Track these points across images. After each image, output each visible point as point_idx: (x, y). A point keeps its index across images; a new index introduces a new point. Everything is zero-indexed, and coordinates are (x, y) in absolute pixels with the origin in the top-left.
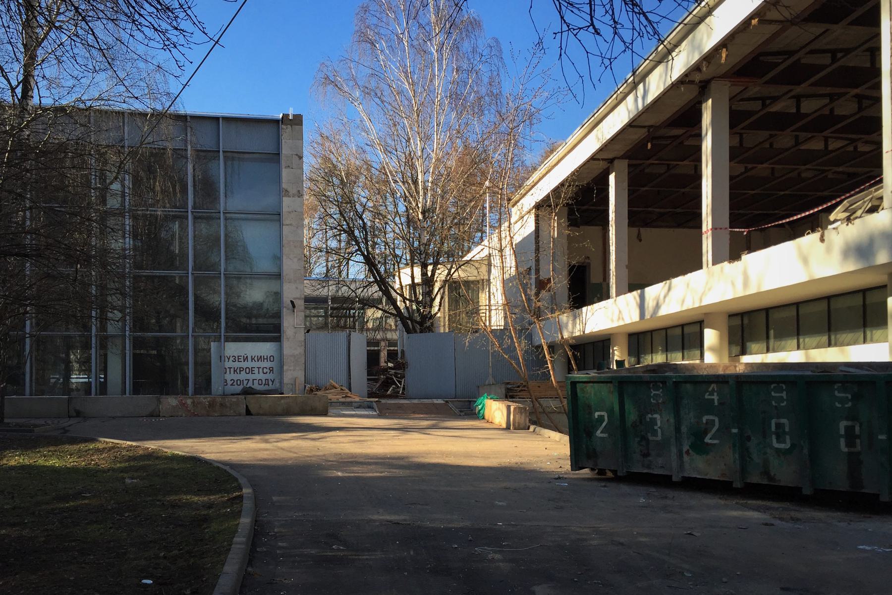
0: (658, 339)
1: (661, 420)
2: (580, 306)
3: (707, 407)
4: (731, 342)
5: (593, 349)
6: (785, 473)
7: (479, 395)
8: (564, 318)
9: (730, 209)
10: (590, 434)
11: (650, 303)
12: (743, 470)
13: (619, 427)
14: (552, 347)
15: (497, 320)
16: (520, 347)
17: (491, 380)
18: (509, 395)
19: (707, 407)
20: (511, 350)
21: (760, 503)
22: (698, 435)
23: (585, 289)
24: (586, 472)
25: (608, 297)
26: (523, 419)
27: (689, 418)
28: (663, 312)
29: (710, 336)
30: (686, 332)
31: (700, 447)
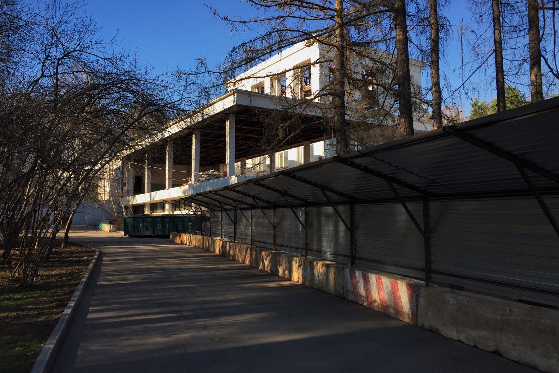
0: (159, 205)
1: (141, 225)
2: (135, 195)
3: (148, 222)
4: (172, 208)
5: (139, 208)
6: (160, 233)
7: (99, 224)
8: (130, 197)
9: (236, 133)
10: (128, 228)
11: (152, 197)
12: (154, 233)
13: (134, 227)
14: (126, 208)
15: (106, 197)
16: (115, 208)
17: (104, 218)
18: (110, 223)
19: (148, 222)
20: (112, 209)
21: (263, 280)
22: (147, 227)
23: (139, 190)
24: (127, 236)
25: (144, 192)
26: (115, 229)
27: (146, 224)
28: (155, 200)
29: (167, 206)
30: (161, 205)
31: (147, 229)
